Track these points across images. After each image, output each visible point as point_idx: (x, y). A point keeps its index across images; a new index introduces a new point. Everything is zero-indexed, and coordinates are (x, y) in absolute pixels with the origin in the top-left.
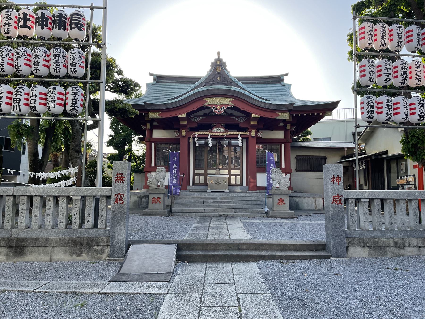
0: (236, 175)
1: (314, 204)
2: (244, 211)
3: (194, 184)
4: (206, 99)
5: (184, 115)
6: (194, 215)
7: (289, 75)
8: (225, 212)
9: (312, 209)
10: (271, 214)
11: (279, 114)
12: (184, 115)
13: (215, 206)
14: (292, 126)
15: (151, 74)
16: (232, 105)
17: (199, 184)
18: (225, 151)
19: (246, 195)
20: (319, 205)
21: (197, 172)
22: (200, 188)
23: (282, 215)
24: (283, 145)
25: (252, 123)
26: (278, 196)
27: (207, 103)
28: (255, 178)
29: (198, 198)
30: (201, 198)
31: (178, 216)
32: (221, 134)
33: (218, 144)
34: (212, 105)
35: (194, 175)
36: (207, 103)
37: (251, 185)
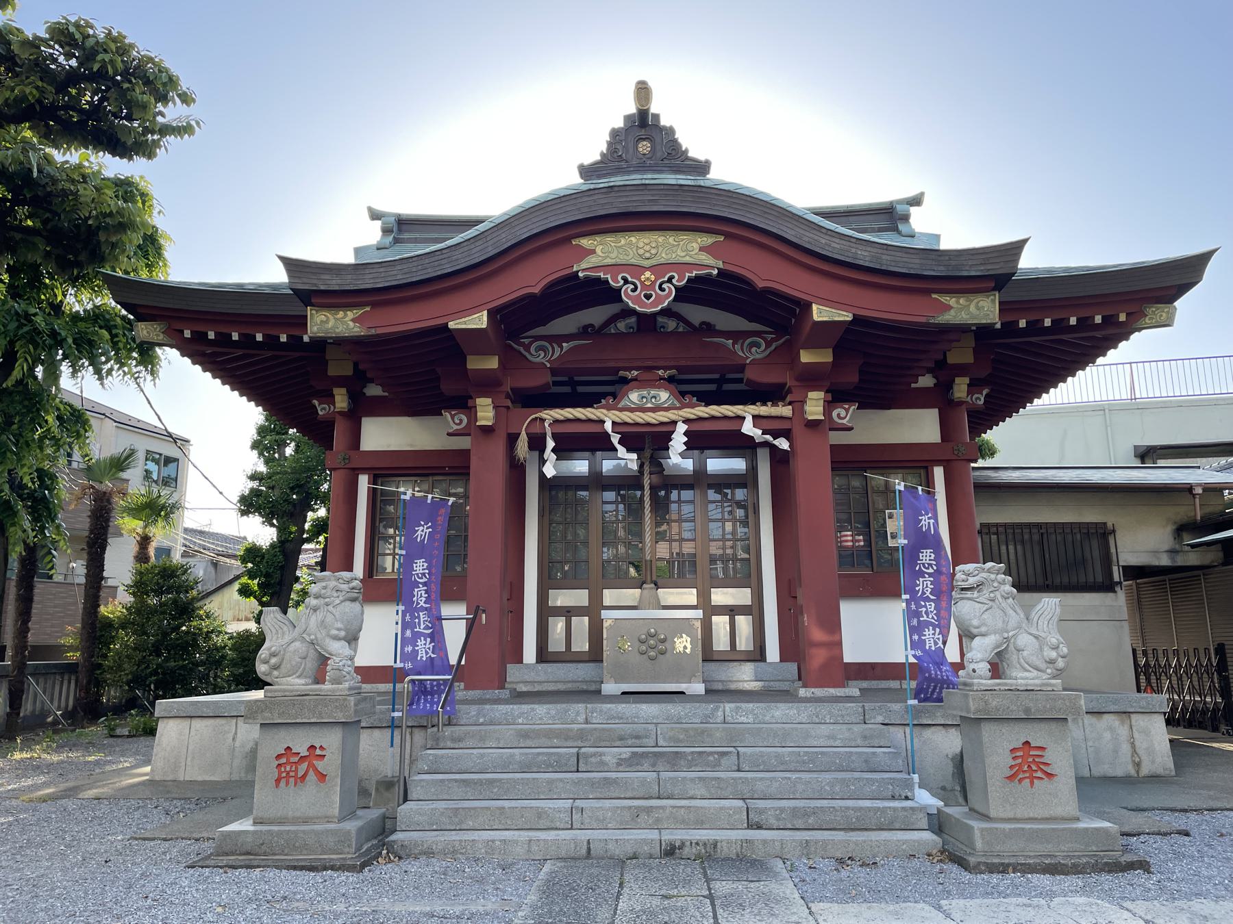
0: (732, 611)
1: (1125, 748)
2: (806, 813)
3: (543, 655)
4: (585, 242)
5: (479, 320)
6: (520, 850)
7: (926, 200)
8: (700, 824)
9: (1119, 772)
10: (979, 844)
11: (945, 299)
12: (479, 320)
13: (643, 782)
14: (973, 386)
15: (375, 215)
16: (712, 265)
17: (568, 657)
18: (680, 521)
19: (803, 717)
20: (1150, 751)
21: (561, 598)
22: (571, 676)
23: (1048, 848)
24: (938, 473)
25: (806, 357)
26: (1005, 729)
27: (591, 261)
28: (833, 624)
29: (549, 734)
30: (565, 735)
31: (429, 853)
32: (662, 417)
33: (647, 469)
34: (615, 267)
35: (545, 612)
36: (591, 261)
37: (810, 656)
